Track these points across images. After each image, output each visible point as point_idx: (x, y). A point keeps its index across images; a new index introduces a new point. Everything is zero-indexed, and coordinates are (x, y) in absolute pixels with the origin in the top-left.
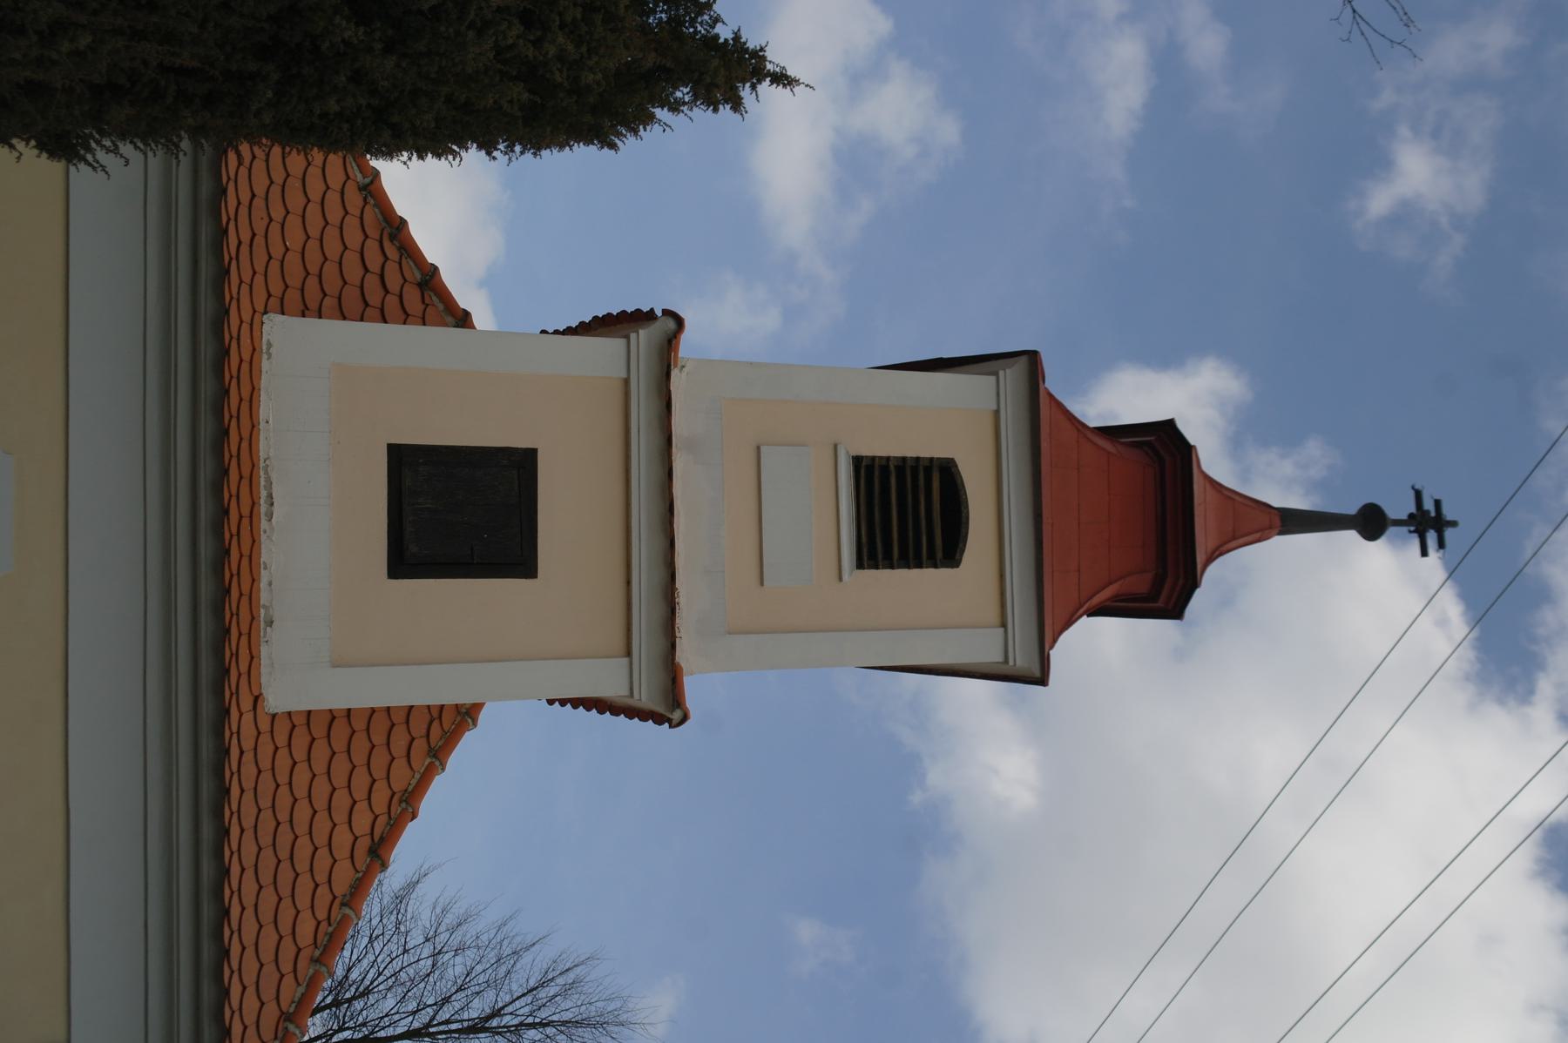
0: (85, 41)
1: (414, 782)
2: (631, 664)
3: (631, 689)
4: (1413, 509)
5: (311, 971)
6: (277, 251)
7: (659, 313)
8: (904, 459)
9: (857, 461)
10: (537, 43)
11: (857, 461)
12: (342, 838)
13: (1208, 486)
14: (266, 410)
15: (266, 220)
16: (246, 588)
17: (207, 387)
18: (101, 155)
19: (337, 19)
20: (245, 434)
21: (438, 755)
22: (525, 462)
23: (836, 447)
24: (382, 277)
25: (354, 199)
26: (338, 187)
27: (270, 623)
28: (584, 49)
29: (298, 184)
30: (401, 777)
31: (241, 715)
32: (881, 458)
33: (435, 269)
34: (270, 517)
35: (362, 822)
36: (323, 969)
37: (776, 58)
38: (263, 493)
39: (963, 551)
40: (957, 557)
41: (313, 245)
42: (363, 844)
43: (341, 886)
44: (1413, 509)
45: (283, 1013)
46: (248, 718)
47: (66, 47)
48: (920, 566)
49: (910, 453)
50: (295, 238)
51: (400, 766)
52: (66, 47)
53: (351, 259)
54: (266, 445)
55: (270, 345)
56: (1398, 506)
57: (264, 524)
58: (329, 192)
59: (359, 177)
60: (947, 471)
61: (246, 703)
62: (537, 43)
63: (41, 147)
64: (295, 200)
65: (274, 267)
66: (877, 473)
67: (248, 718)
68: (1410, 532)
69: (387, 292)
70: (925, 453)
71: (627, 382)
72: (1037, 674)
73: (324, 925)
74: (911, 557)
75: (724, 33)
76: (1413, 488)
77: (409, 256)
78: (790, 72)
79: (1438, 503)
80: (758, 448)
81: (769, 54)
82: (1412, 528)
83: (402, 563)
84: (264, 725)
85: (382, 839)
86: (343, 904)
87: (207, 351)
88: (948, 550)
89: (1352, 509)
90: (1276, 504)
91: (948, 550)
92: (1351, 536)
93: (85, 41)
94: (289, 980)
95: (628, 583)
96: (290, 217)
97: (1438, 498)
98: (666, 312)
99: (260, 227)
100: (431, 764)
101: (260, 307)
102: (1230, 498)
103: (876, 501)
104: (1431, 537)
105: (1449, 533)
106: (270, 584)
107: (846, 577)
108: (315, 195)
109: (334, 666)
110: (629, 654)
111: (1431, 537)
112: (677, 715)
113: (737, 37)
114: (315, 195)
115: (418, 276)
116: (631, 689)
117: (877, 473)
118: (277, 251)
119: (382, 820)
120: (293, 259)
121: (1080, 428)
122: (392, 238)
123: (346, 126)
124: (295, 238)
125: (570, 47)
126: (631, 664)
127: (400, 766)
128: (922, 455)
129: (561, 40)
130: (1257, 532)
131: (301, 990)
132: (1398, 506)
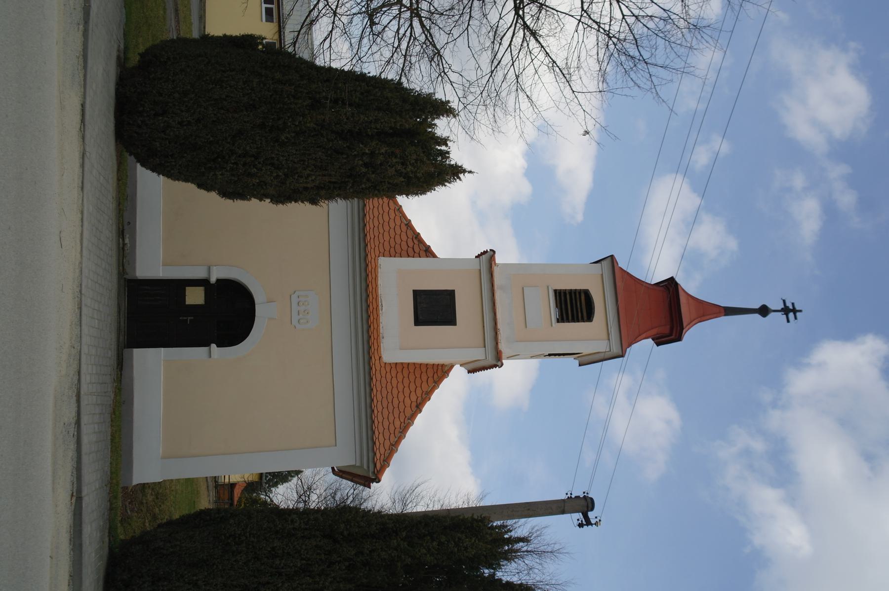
0: (314, 177)
1: (429, 390)
2: (485, 349)
3: (486, 357)
4: (783, 307)
5: (399, 435)
6: (382, 241)
7: (489, 250)
8: (571, 290)
9: (555, 291)
10: (405, 169)
11: (555, 291)
12: (407, 401)
13: (689, 298)
14: (380, 282)
15: (378, 233)
16: (376, 327)
17: (363, 275)
18: (321, 203)
19: (361, 168)
20: (374, 287)
21: (437, 383)
22: (451, 294)
23: (548, 287)
24: (413, 248)
25: (404, 228)
26: (393, 218)
27: (383, 338)
28: (416, 168)
29: (387, 224)
30: (425, 387)
31: (375, 360)
32: (563, 290)
33: (429, 246)
34: (382, 310)
35: (414, 398)
36: (403, 435)
37: (466, 166)
38: (380, 304)
39: (593, 317)
40: (591, 319)
41: (392, 240)
42: (414, 404)
43: (408, 414)
44: (783, 307)
45: (391, 444)
46: (377, 362)
47: (310, 179)
48: (578, 322)
49: (573, 288)
50: (387, 237)
51: (424, 384)
52: (310, 179)
53: (404, 244)
54: (381, 291)
55: (380, 265)
56: (775, 304)
57: (380, 312)
58: (396, 226)
59: (405, 222)
60: (587, 293)
61: (377, 358)
62: (405, 169)
63: (310, 203)
64: (386, 228)
65: (381, 245)
66: (568, 296)
67: (377, 362)
68: (782, 314)
69: (415, 252)
70: (578, 288)
71: (480, 270)
72: (621, 354)
73: (403, 424)
74: (575, 319)
75: (453, 163)
76: (782, 299)
77: (421, 243)
78: (473, 171)
79: (793, 304)
80: (523, 288)
81: (463, 166)
82: (783, 313)
83: (418, 322)
84: (383, 365)
85: (420, 404)
86: (408, 419)
87: (363, 265)
88: (589, 315)
89: (757, 306)
90: (722, 305)
91: (589, 315)
92: (757, 316)
93: (314, 177)
94: (392, 435)
95: (484, 327)
96: (385, 232)
97: (793, 302)
98: (490, 250)
99: (376, 235)
100: (434, 385)
101: (377, 255)
102: (700, 302)
103: (579, 310)
104: (791, 315)
105: (798, 314)
106: (383, 327)
107: (553, 325)
108: (392, 227)
109: (401, 349)
110: (485, 347)
111: (791, 315)
112: (499, 364)
113: (456, 164)
114: (392, 227)
115: (424, 249)
116: (486, 357)
117: (568, 296)
118: (382, 241)
119: (420, 399)
120: (386, 244)
121: (639, 282)
122: (416, 238)
123: (367, 191)
124: (387, 237)
125: (412, 168)
126: (485, 349)
127: (424, 384)
128: (577, 288)
129: (410, 167)
130: (715, 314)
131: (396, 439)
132: (775, 304)
